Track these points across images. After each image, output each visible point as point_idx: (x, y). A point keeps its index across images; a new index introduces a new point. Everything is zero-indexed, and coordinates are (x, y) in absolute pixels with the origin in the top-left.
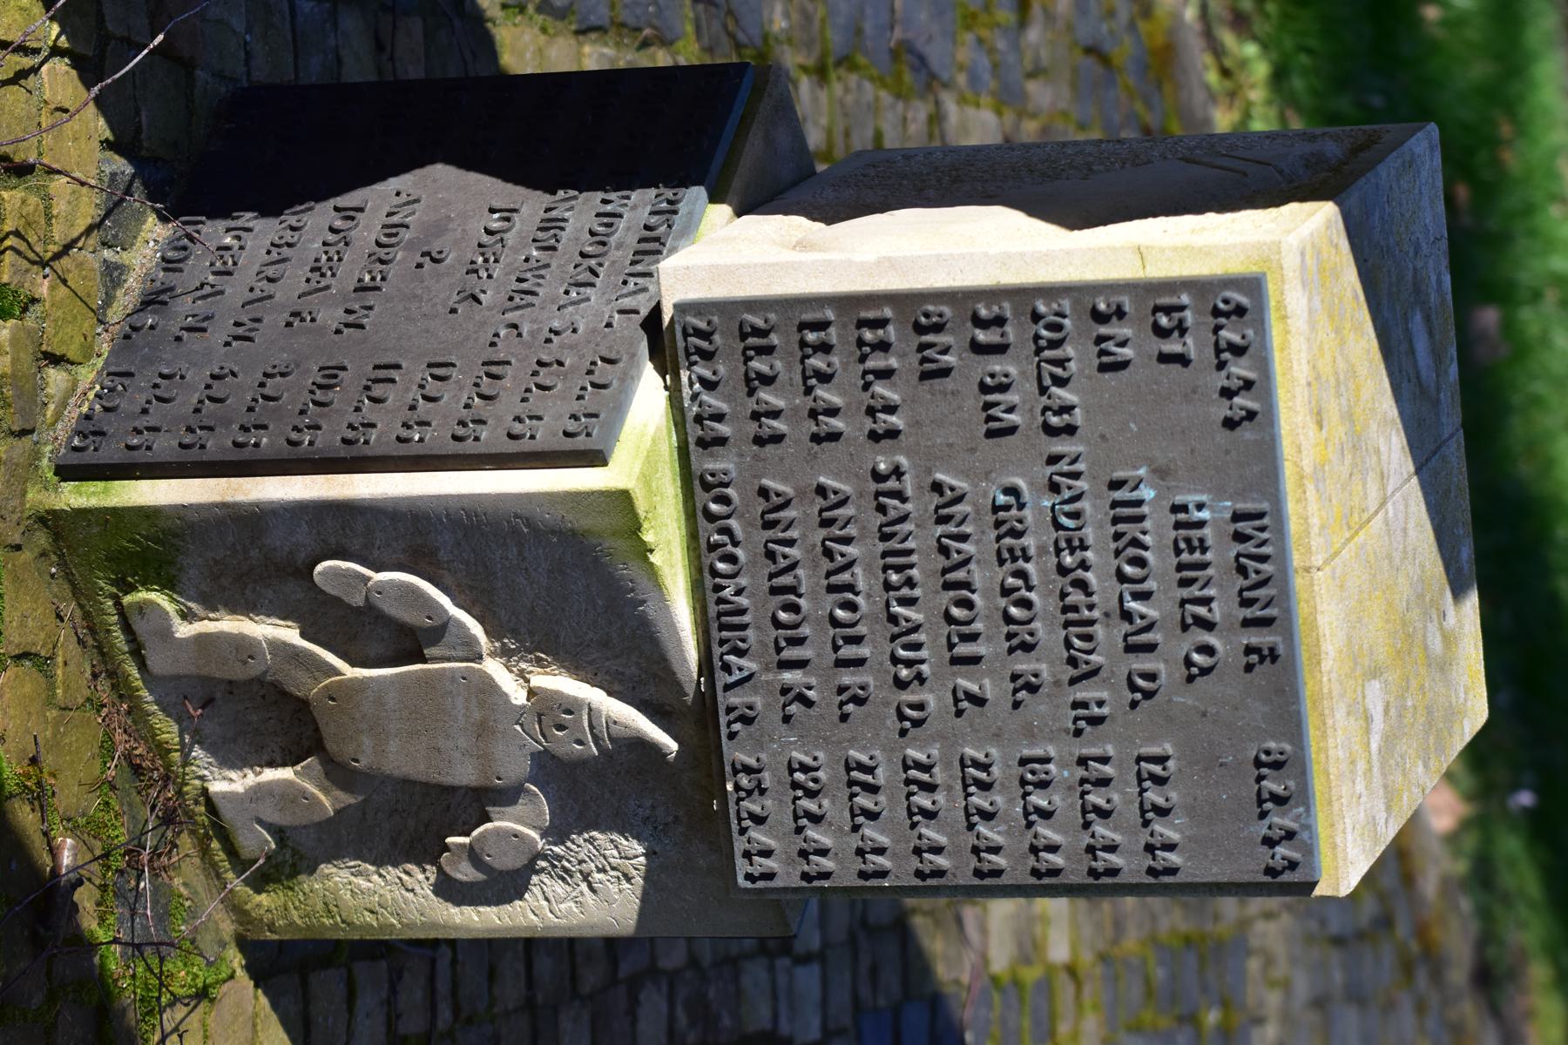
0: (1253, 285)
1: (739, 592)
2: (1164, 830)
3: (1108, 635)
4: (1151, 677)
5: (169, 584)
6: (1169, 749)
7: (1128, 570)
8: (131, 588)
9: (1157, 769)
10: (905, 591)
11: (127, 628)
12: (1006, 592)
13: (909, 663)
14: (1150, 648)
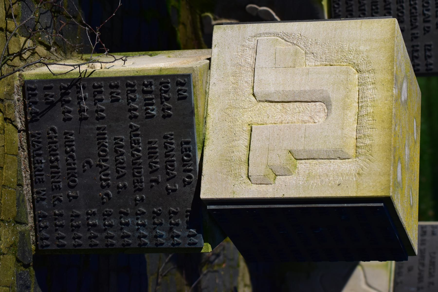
0: (188, 76)
1: (340, 11)
2: (430, 61)
3: (420, 19)
4: (429, 27)
5: (212, 12)
6: (431, 43)
7: (425, 5)
8: (203, 12)
9: (429, 48)
10: (376, 11)
11: (201, 22)
12: (398, 10)
13: (105, 180)
14: (429, 21)
